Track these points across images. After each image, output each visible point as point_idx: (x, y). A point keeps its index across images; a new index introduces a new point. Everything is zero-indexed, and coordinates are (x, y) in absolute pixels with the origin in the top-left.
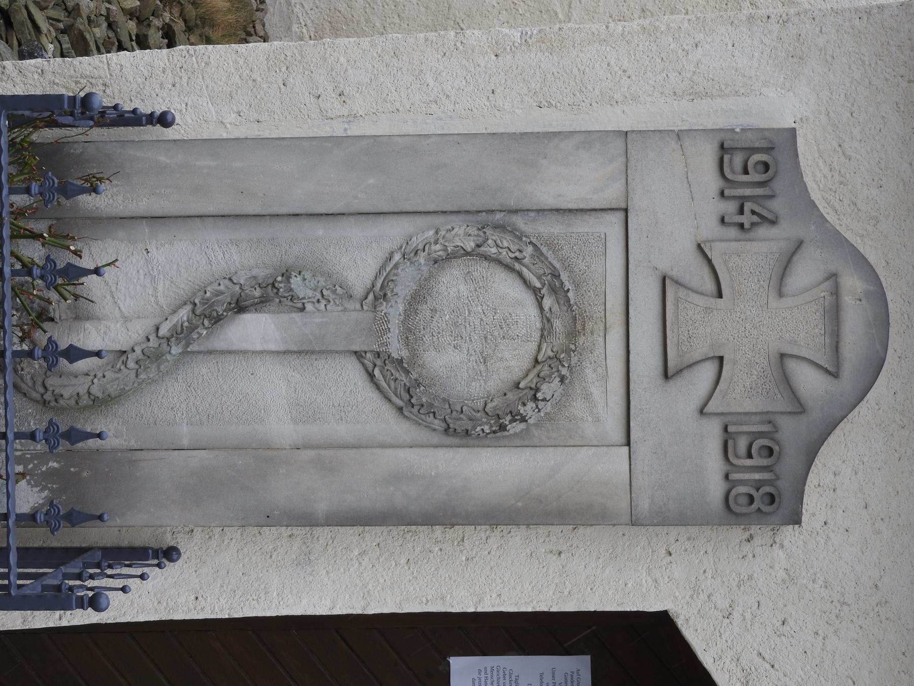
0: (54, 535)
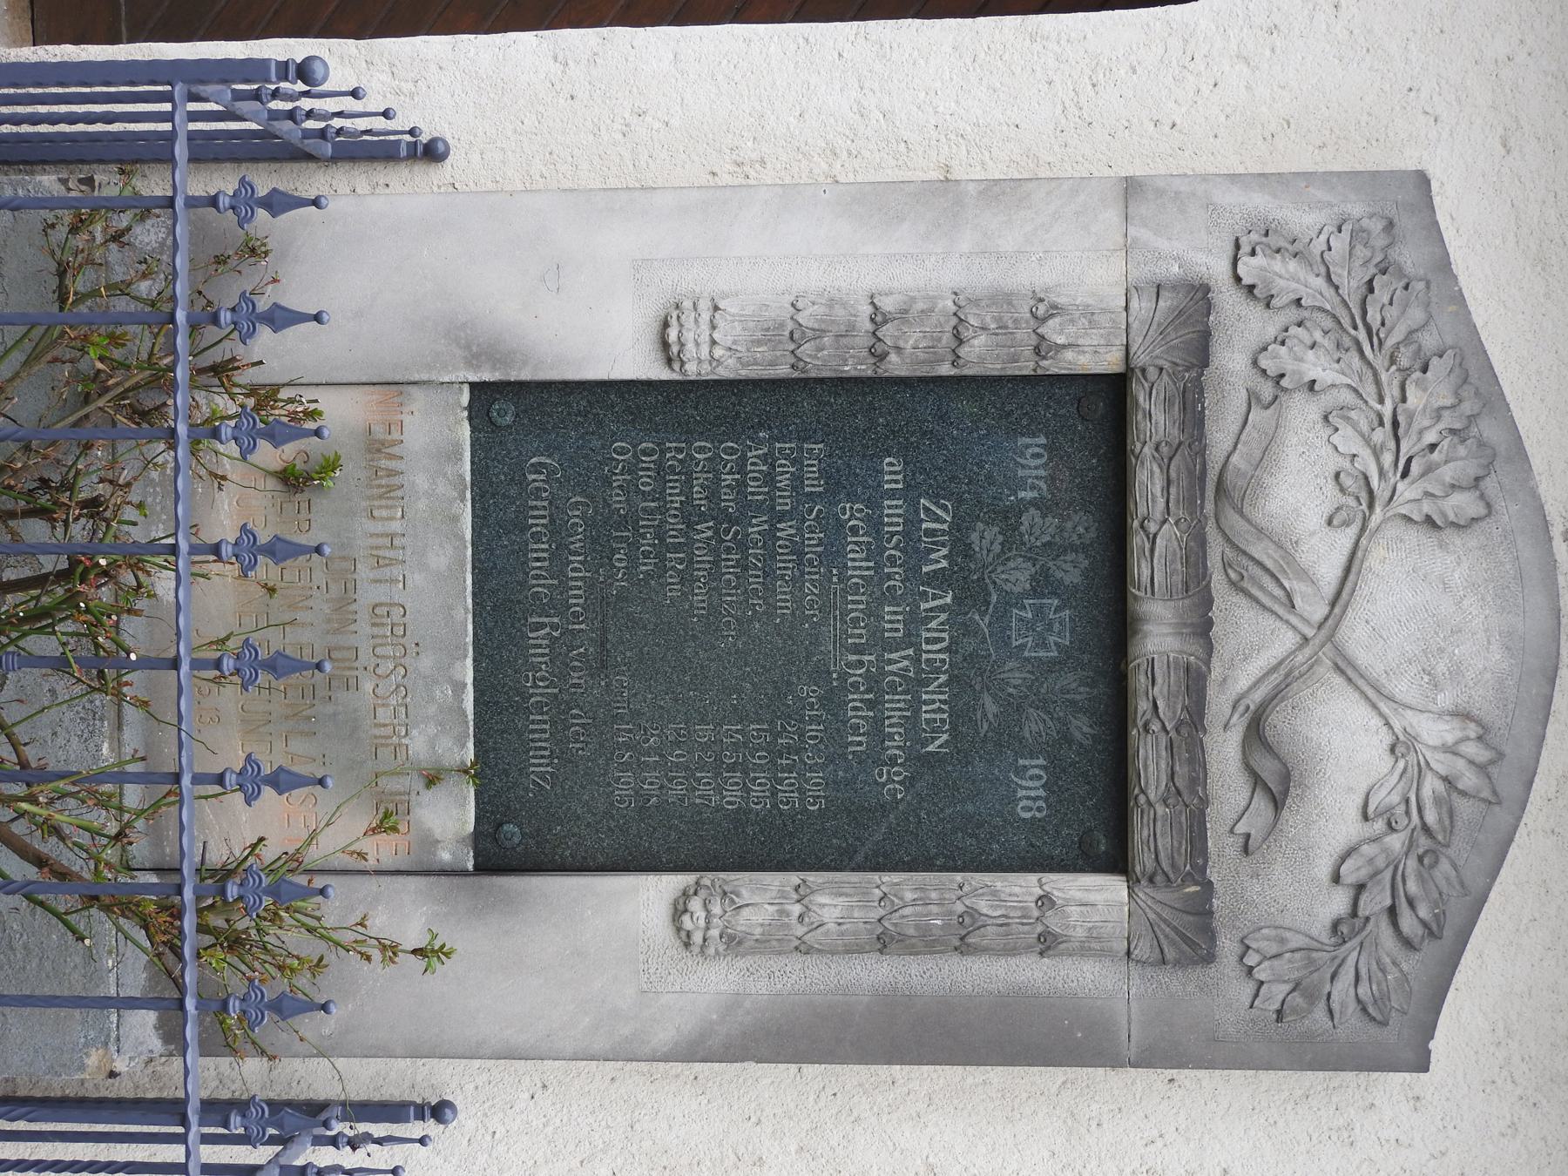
0: (245, 344)
